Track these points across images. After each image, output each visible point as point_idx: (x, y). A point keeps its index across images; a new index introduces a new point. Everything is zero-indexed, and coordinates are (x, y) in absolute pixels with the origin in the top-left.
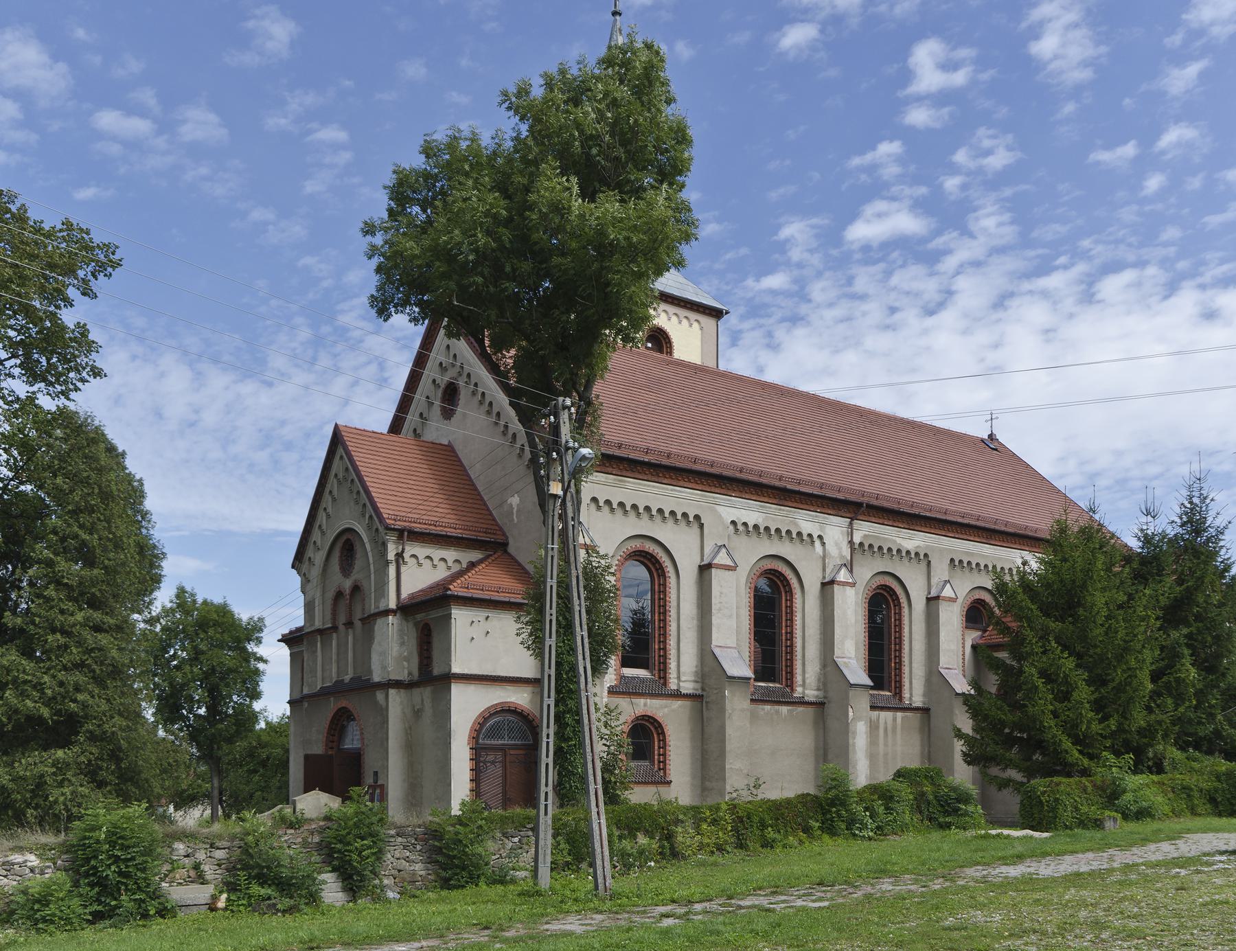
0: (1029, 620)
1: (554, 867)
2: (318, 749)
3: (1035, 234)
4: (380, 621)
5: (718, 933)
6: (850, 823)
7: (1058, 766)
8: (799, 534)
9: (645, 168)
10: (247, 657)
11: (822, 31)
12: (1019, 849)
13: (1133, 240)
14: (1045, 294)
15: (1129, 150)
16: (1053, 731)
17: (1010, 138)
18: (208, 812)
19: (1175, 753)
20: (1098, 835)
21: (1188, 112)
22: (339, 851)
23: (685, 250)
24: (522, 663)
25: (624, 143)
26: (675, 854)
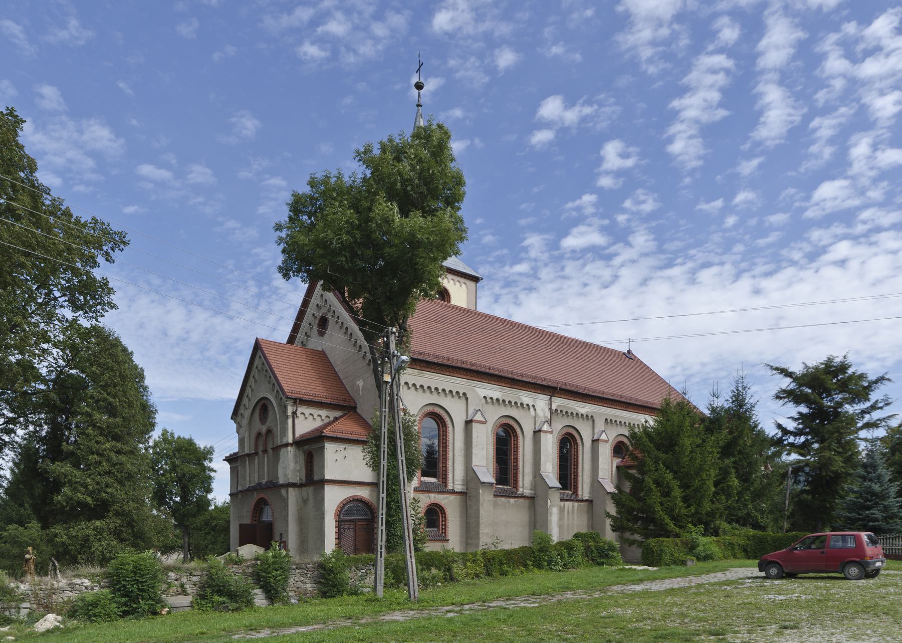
0: (648, 452)
1: (386, 585)
2: (247, 521)
3: (666, 246)
4: (283, 450)
5: (479, 620)
6: (549, 562)
7: (663, 532)
8: (522, 404)
9: (438, 199)
10: (205, 469)
11: (556, 137)
12: (641, 576)
13: (719, 250)
14: (670, 278)
15: (719, 203)
16: (660, 513)
17: (656, 195)
18: (182, 556)
19: (725, 525)
20: (684, 569)
21: (752, 183)
22: (264, 577)
23: (460, 246)
24: (367, 475)
25: (426, 184)
26: (452, 579)
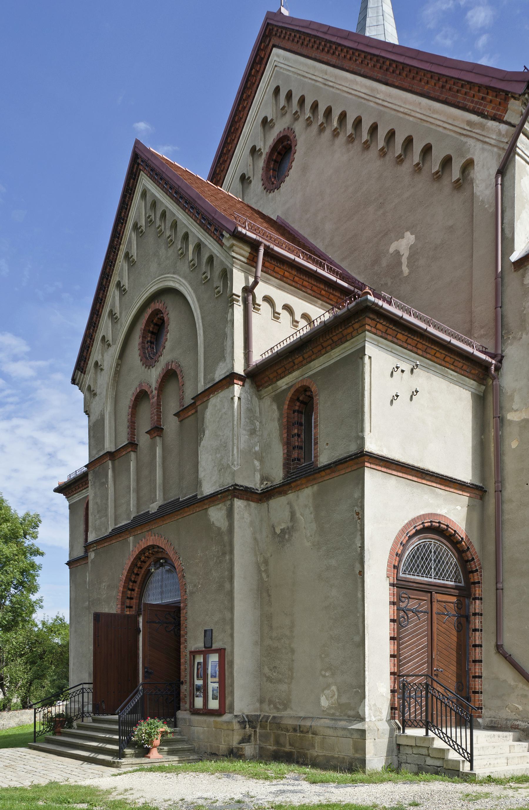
2: (112, 607)
